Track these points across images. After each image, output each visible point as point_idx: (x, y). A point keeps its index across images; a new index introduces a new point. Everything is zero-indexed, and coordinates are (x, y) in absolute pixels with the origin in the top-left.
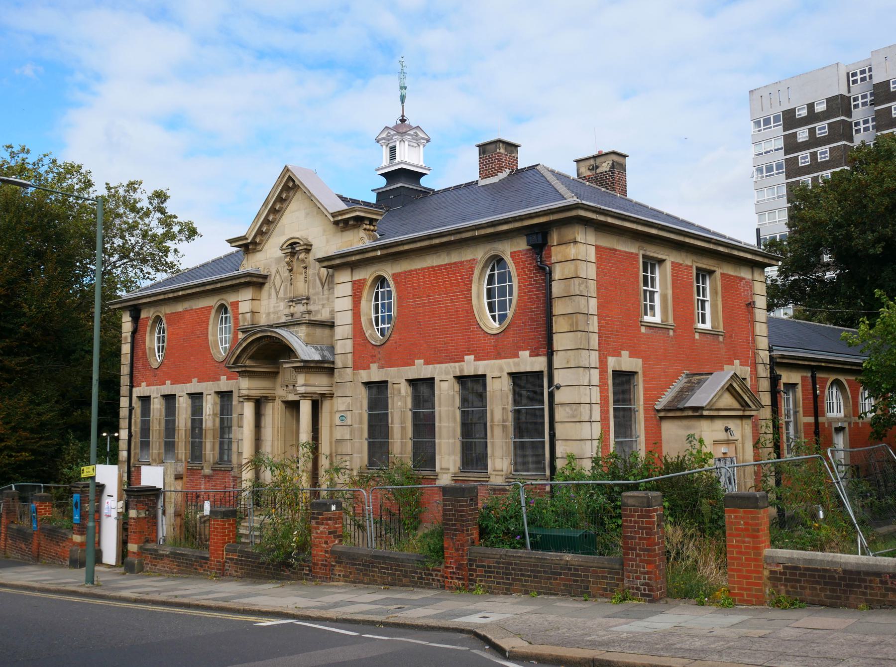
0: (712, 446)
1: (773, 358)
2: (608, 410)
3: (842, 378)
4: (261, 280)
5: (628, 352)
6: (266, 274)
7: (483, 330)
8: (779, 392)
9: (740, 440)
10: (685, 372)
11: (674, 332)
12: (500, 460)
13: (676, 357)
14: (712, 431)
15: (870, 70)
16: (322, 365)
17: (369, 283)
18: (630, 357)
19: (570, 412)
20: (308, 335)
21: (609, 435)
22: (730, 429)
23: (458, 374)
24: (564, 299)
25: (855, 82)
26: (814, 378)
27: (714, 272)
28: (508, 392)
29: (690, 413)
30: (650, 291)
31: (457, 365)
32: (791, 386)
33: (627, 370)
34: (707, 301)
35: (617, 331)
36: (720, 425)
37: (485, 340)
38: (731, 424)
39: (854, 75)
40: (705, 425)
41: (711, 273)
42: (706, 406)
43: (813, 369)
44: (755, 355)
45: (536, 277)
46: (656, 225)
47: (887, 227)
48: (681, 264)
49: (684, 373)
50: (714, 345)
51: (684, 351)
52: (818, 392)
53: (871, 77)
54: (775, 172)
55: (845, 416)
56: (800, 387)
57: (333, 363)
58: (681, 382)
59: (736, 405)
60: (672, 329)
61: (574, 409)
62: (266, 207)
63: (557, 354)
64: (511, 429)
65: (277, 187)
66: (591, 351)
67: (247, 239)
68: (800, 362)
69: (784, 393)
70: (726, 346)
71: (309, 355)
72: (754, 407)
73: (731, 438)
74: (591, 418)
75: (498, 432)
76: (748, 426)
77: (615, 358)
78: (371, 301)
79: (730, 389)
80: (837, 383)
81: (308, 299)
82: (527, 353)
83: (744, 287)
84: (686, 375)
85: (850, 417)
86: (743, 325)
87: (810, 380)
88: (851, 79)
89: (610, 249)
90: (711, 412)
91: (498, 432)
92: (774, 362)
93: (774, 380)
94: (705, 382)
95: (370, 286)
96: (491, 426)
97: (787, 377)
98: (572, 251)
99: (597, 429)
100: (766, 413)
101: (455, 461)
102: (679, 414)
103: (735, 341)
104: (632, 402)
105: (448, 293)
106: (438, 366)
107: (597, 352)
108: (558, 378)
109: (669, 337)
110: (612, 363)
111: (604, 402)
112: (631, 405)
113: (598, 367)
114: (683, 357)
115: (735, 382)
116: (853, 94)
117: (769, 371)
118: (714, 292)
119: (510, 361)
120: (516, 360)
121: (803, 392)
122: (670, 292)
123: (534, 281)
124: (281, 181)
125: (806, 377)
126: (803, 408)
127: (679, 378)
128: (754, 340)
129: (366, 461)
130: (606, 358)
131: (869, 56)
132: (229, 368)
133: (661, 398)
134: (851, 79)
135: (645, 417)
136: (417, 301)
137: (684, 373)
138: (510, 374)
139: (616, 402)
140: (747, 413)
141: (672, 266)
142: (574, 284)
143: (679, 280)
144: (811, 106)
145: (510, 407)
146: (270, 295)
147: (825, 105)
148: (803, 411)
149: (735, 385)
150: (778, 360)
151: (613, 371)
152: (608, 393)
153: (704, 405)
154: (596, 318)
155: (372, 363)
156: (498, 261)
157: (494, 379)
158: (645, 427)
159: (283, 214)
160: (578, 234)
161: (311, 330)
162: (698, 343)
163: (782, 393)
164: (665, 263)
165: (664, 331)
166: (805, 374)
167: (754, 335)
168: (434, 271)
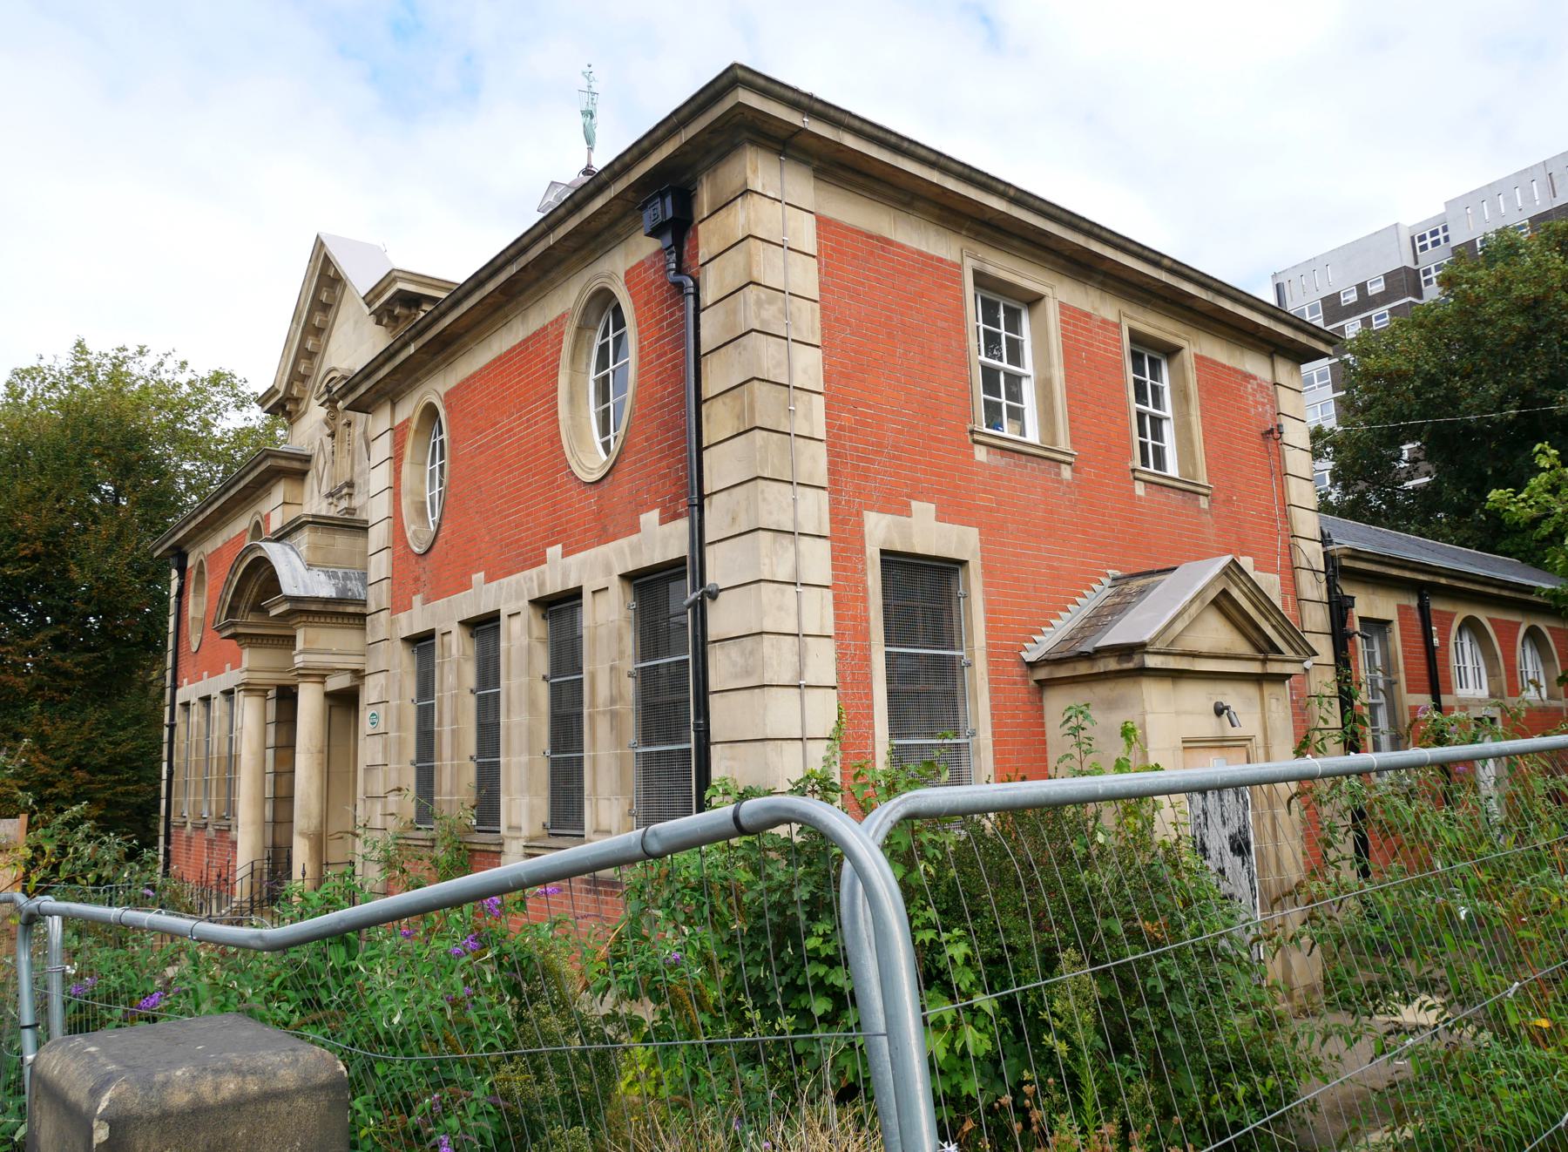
0: (1180, 753)
1: (1333, 557)
2: (867, 658)
3: (1482, 615)
4: (296, 465)
5: (933, 506)
6: (306, 453)
7: (577, 478)
8: (1351, 636)
9: (1259, 738)
10: (1109, 571)
11: (1074, 470)
12: (606, 802)
13: (1085, 533)
14: (1178, 713)
15: (1445, 229)
16: (340, 609)
17: (414, 425)
18: (939, 519)
19: (740, 661)
20: (313, 548)
21: (872, 726)
22: (1227, 708)
23: (537, 595)
24: (723, 350)
25: (1424, 248)
26: (1424, 609)
27: (1178, 349)
28: (623, 624)
29: (1112, 664)
30: (1008, 375)
31: (534, 572)
32: (1376, 626)
33: (933, 553)
34: (1168, 419)
35: (895, 448)
36: (1198, 697)
37: (580, 502)
38: (1232, 695)
39: (1423, 238)
40: (1153, 694)
41: (1171, 352)
42: (1153, 641)
43: (1424, 591)
44: (1290, 549)
45: (672, 314)
46: (1002, 187)
47: (1522, 372)
48: (1088, 315)
49: (1107, 575)
50: (1187, 516)
51: (1104, 522)
52: (1436, 641)
53: (1447, 239)
54: (1316, 384)
55: (1492, 695)
56: (1396, 627)
57: (364, 603)
58: (1099, 594)
59: (1243, 647)
60: (1070, 464)
61: (747, 652)
62: (298, 324)
63: (710, 504)
64: (631, 723)
65: (310, 282)
66: (800, 489)
67: (277, 391)
68: (1395, 572)
69: (1363, 637)
70: (1216, 522)
71: (305, 587)
72: (1290, 654)
73: (1232, 732)
74: (801, 675)
75: (603, 726)
76: (1278, 703)
77: (889, 517)
78: (424, 464)
79: (1223, 604)
80: (1470, 625)
81: (350, 485)
82: (655, 515)
83: (1254, 395)
84: (1114, 580)
85: (1502, 697)
86: (1258, 480)
87: (1417, 615)
88: (1418, 245)
89: (871, 237)
90: (1171, 659)
91: (603, 726)
92: (1334, 568)
93: (1339, 608)
94: (1153, 589)
95: (416, 431)
96: (591, 716)
97: (1367, 604)
98: (740, 218)
99: (823, 712)
100: (1323, 680)
101: (532, 811)
102: (1083, 669)
103: (1239, 513)
104: (957, 644)
105: (522, 408)
106: (505, 581)
107: (825, 495)
108: (715, 575)
109: (1060, 482)
110: (880, 531)
111: (848, 634)
112: (953, 649)
113: (826, 532)
114: (1104, 537)
115: (1237, 585)
116: (1422, 267)
117: (1324, 585)
118: (1181, 396)
119: (623, 543)
120: (634, 538)
121: (1403, 641)
122: (1058, 374)
123: (669, 325)
124: (315, 268)
125: (1408, 608)
126: (1407, 674)
127: (1094, 586)
128: (1286, 517)
129: (543, 814)
130: (859, 514)
131: (1442, 209)
132: (219, 630)
133: (1042, 633)
134: (1418, 243)
135: (991, 681)
136: (477, 441)
137: (1107, 575)
138: (626, 577)
139: (892, 635)
140: (1274, 668)
141: (1062, 313)
142: (745, 302)
143: (1083, 350)
144: (1362, 288)
145: (629, 664)
146: (312, 492)
147: (1383, 283)
148: (1407, 680)
149: (1235, 593)
150: (1345, 562)
151: (883, 552)
152: (866, 609)
153: (1146, 638)
154: (819, 402)
155: (414, 594)
156: (603, 301)
157: (598, 596)
158: (993, 707)
159: (329, 337)
160: (755, 171)
161: (321, 538)
162: (1143, 507)
163: (1358, 639)
164: (1041, 305)
165: (1045, 465)
166: (1405, 602)
167: (1285, 506)
168: (503, 364)
